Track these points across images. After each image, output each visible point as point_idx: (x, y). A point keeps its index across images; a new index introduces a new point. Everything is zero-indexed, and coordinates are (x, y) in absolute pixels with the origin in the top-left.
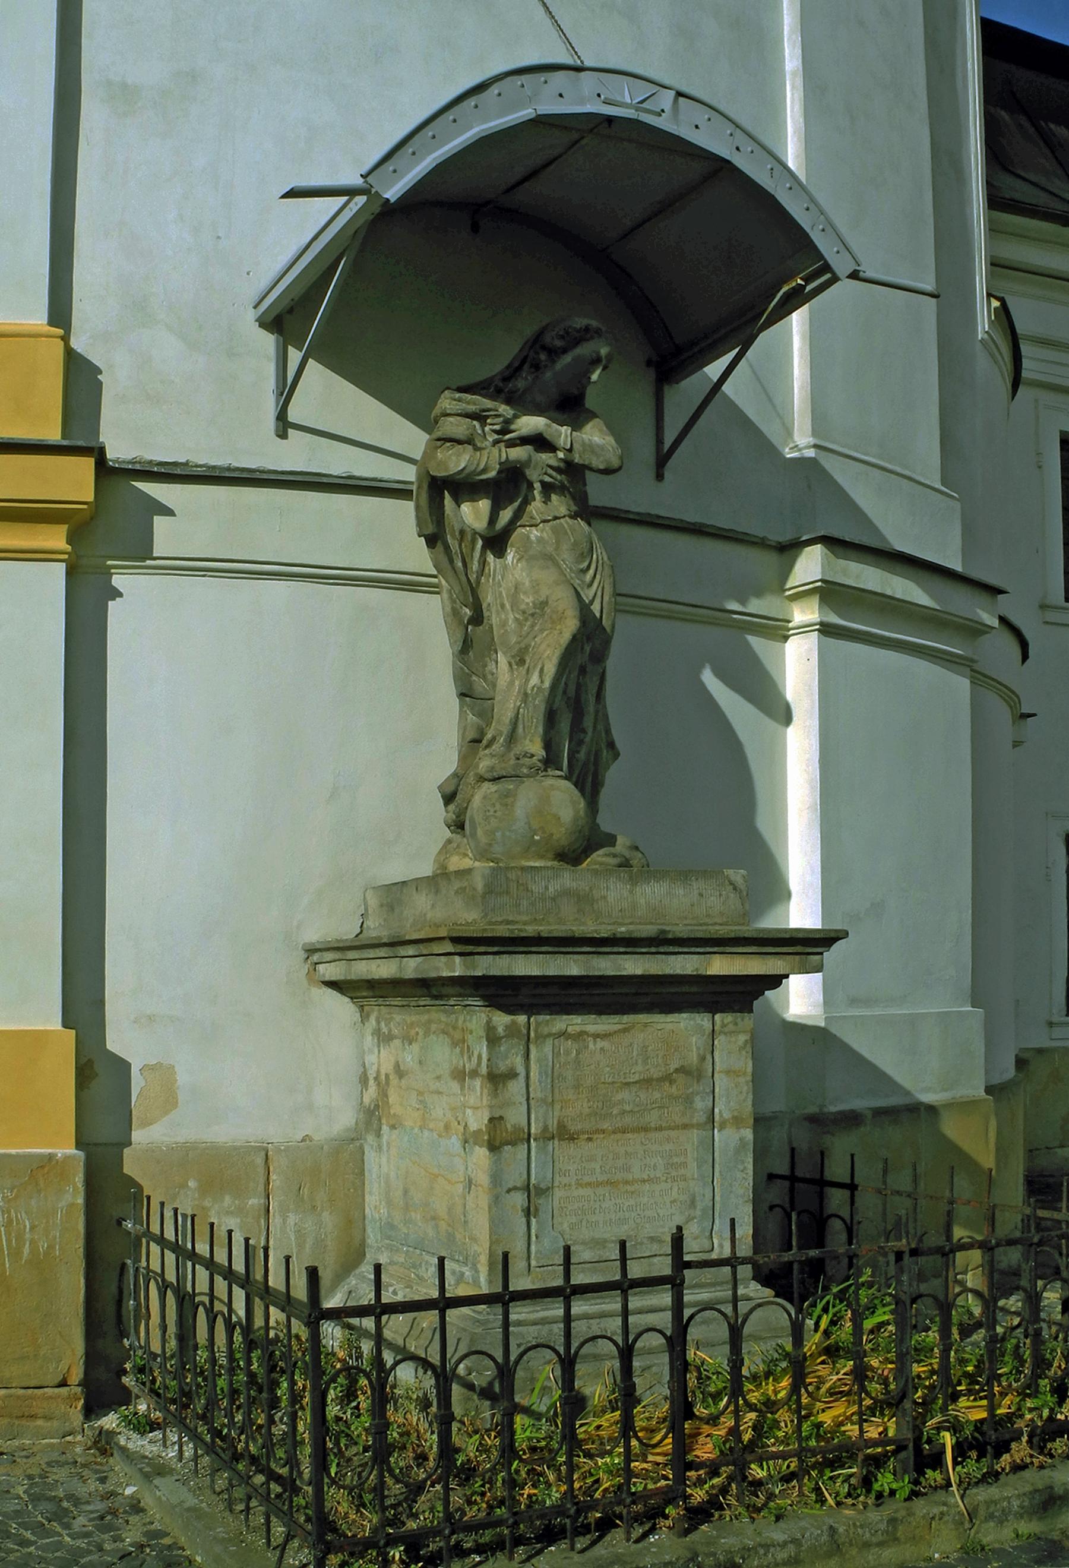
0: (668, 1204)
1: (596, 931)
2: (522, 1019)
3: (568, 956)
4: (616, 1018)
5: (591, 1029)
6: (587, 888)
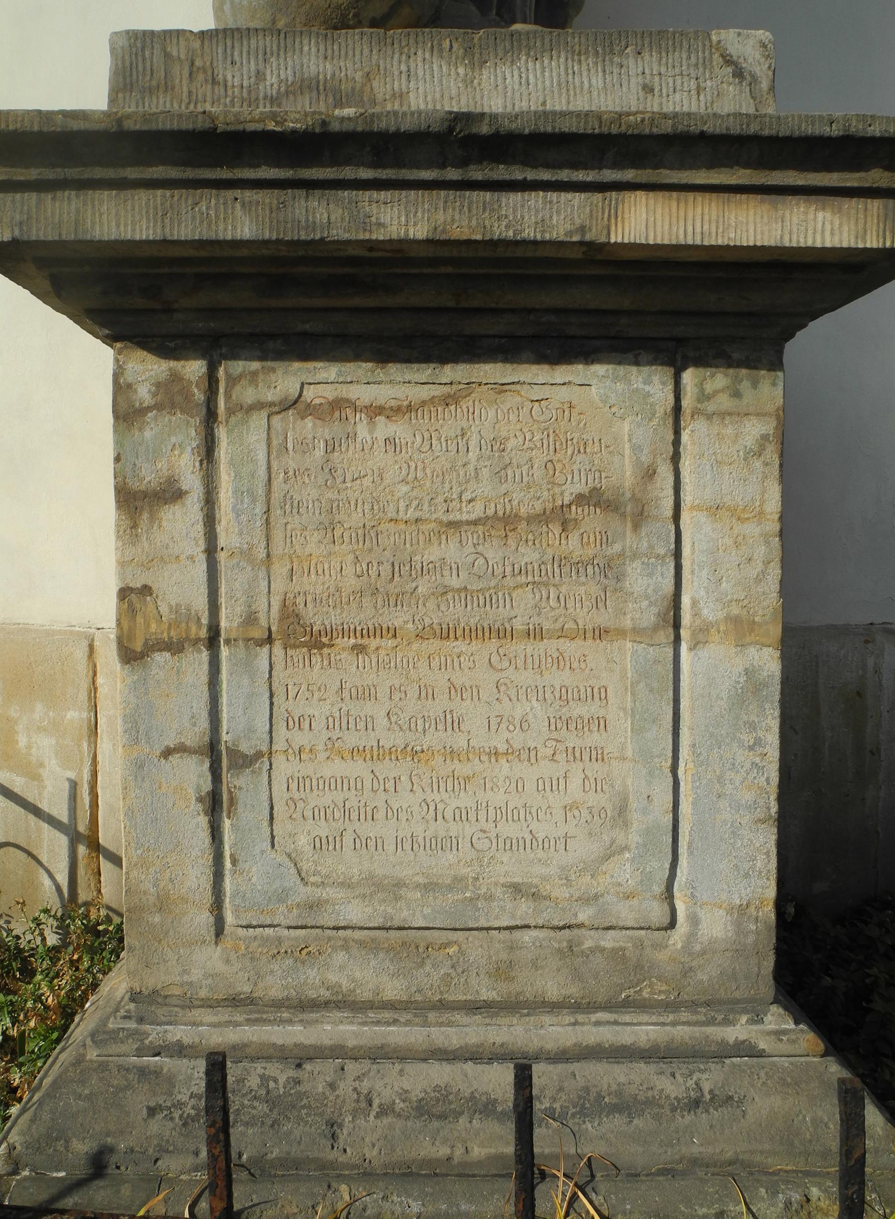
0: (559, 814)
1: (273, 116)
2: (194, 368)
3: (230, 194)
4: (425, 372)
5: (363, 394)
6: (358, 76)
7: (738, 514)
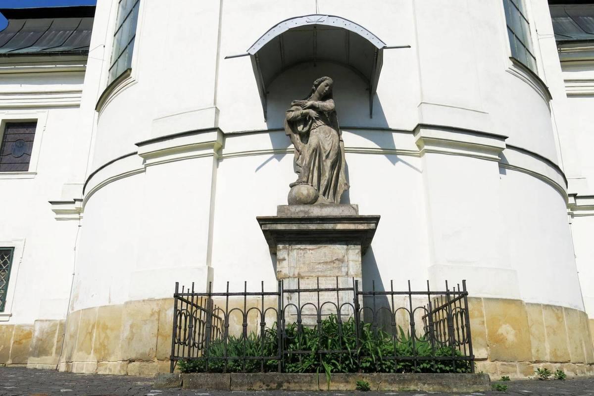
5: (302, 247)
7: (356, 261)
